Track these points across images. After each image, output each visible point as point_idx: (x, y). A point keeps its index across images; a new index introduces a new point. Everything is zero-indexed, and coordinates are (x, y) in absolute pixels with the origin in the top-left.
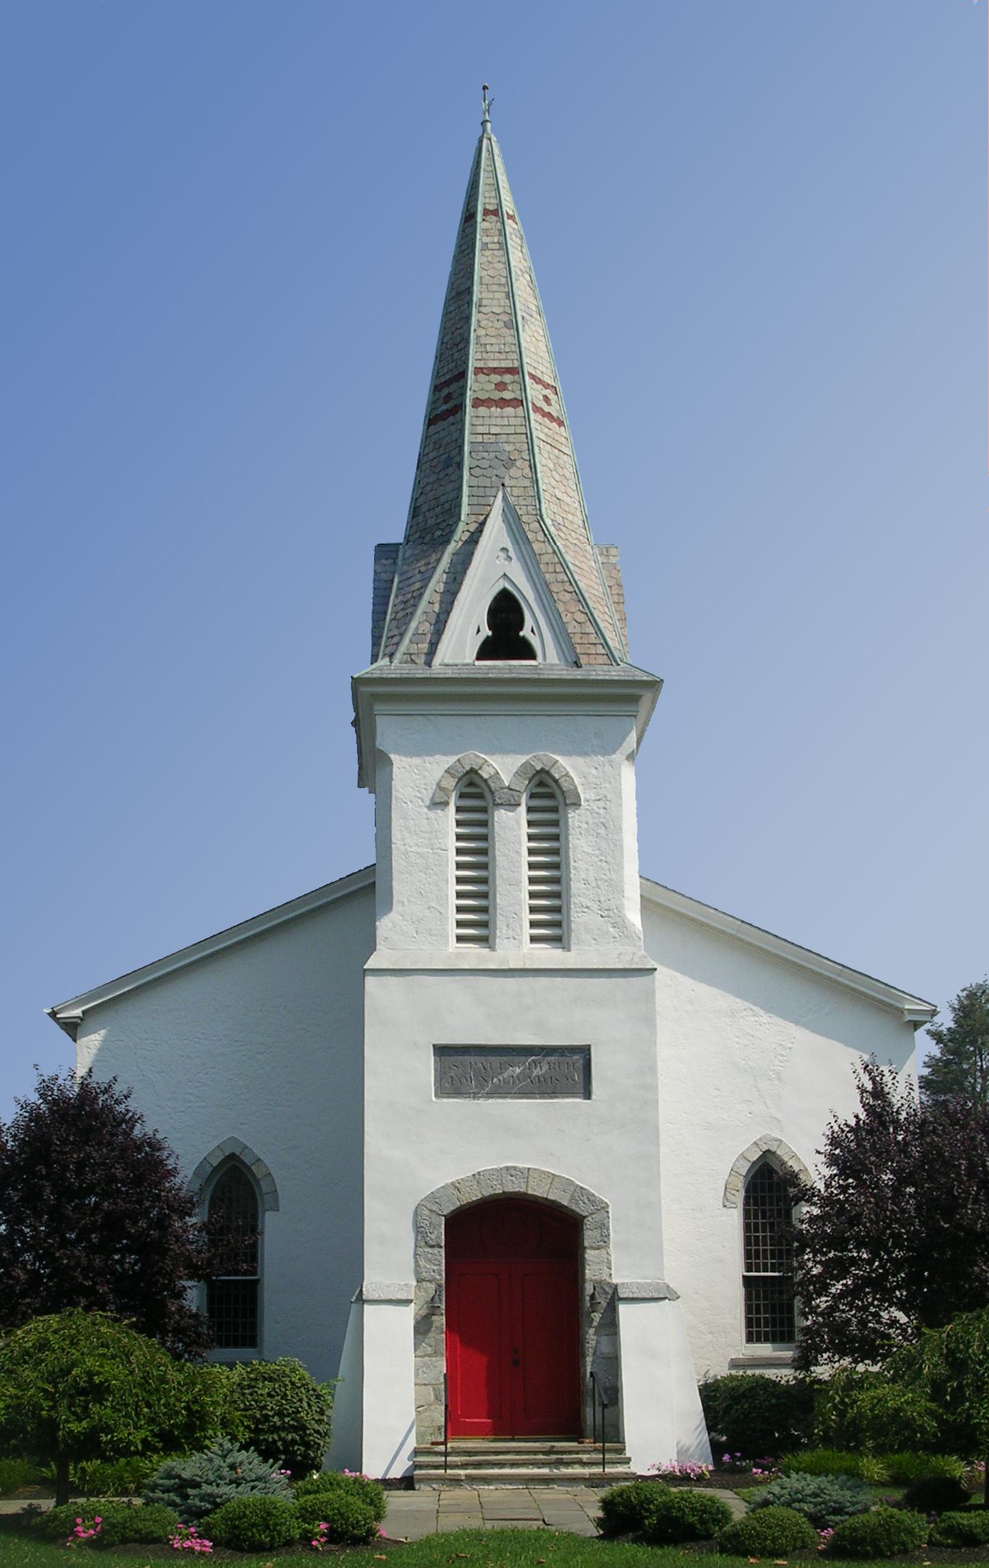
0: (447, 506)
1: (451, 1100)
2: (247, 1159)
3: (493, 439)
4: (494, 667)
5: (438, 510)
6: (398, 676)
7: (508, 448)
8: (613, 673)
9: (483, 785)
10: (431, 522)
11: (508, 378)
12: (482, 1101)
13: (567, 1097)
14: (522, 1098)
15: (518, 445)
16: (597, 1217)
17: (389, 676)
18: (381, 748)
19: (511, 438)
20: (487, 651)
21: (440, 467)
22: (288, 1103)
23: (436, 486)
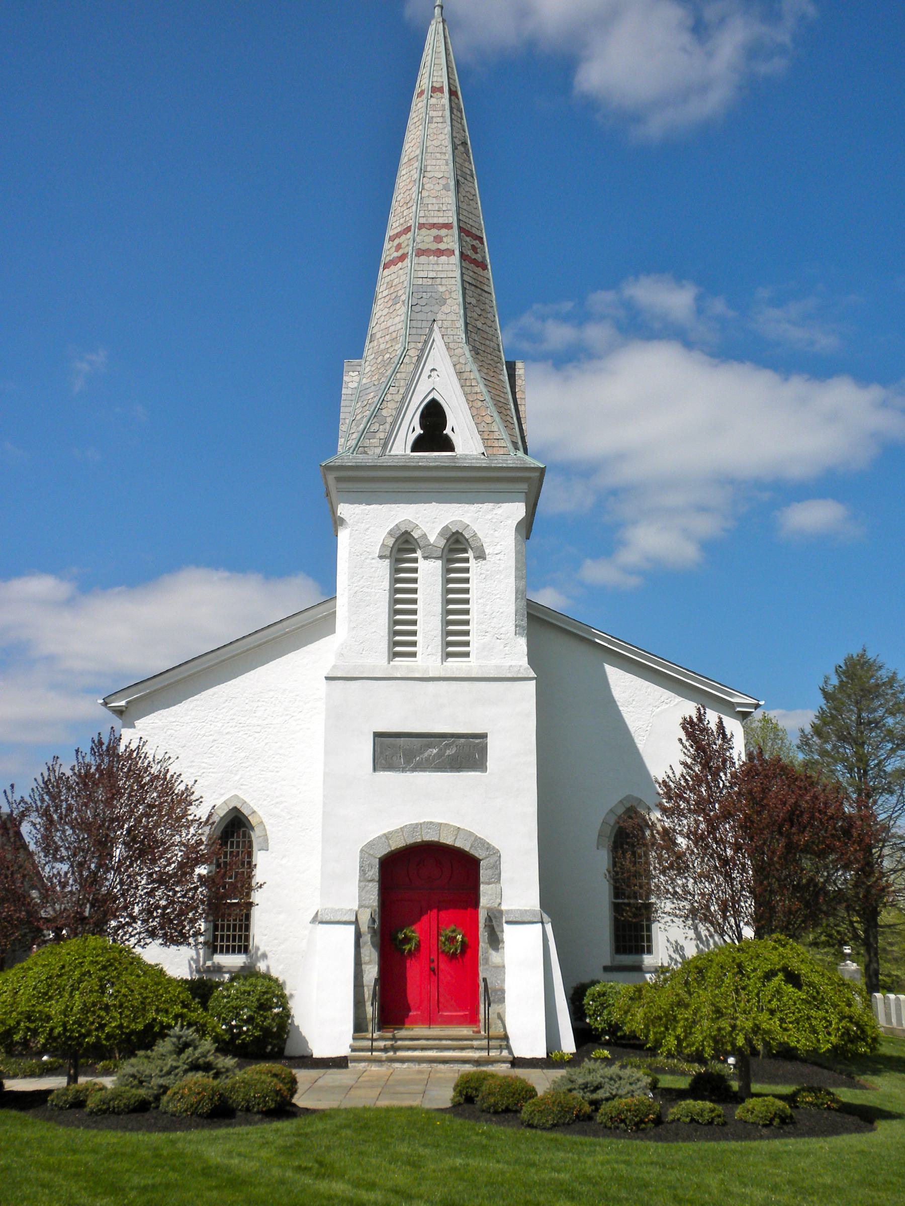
0: (394, 335)
1: (386, 773)
2: (246, 812)
3: (430, 282)
4: (424, 457)
5: (388, 337)
6: (354, 464)
7: (442, 289)
8: (509, 462)
9: (415, 543)
10: (382, 347)
11: (443, 232)
12: (408, 774)
13: (471, 771)
14: (438, 771)
15: (449, 287)
16: (492, 860)
17: (347, 464)
18: (341, 516)
19: (211, 774)
20: (418, 446)
21: (390, 303)
22: (277, 769)
23: (387, 317)
